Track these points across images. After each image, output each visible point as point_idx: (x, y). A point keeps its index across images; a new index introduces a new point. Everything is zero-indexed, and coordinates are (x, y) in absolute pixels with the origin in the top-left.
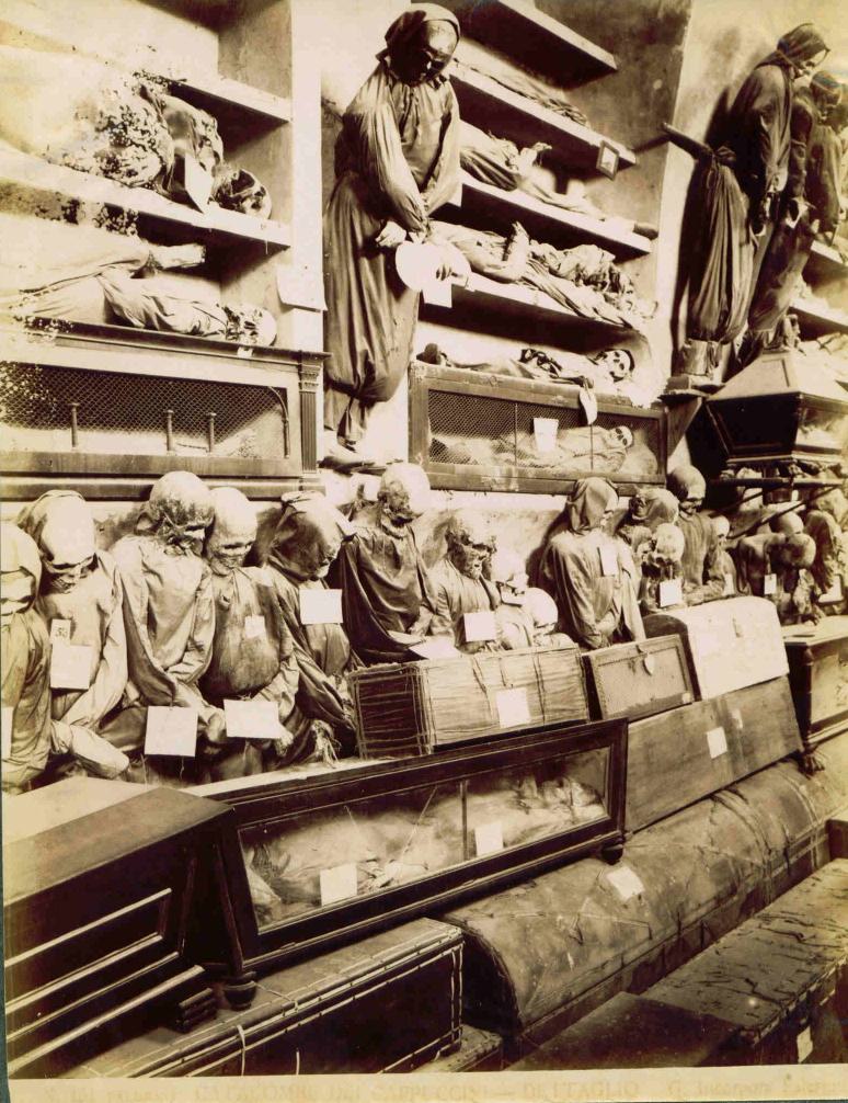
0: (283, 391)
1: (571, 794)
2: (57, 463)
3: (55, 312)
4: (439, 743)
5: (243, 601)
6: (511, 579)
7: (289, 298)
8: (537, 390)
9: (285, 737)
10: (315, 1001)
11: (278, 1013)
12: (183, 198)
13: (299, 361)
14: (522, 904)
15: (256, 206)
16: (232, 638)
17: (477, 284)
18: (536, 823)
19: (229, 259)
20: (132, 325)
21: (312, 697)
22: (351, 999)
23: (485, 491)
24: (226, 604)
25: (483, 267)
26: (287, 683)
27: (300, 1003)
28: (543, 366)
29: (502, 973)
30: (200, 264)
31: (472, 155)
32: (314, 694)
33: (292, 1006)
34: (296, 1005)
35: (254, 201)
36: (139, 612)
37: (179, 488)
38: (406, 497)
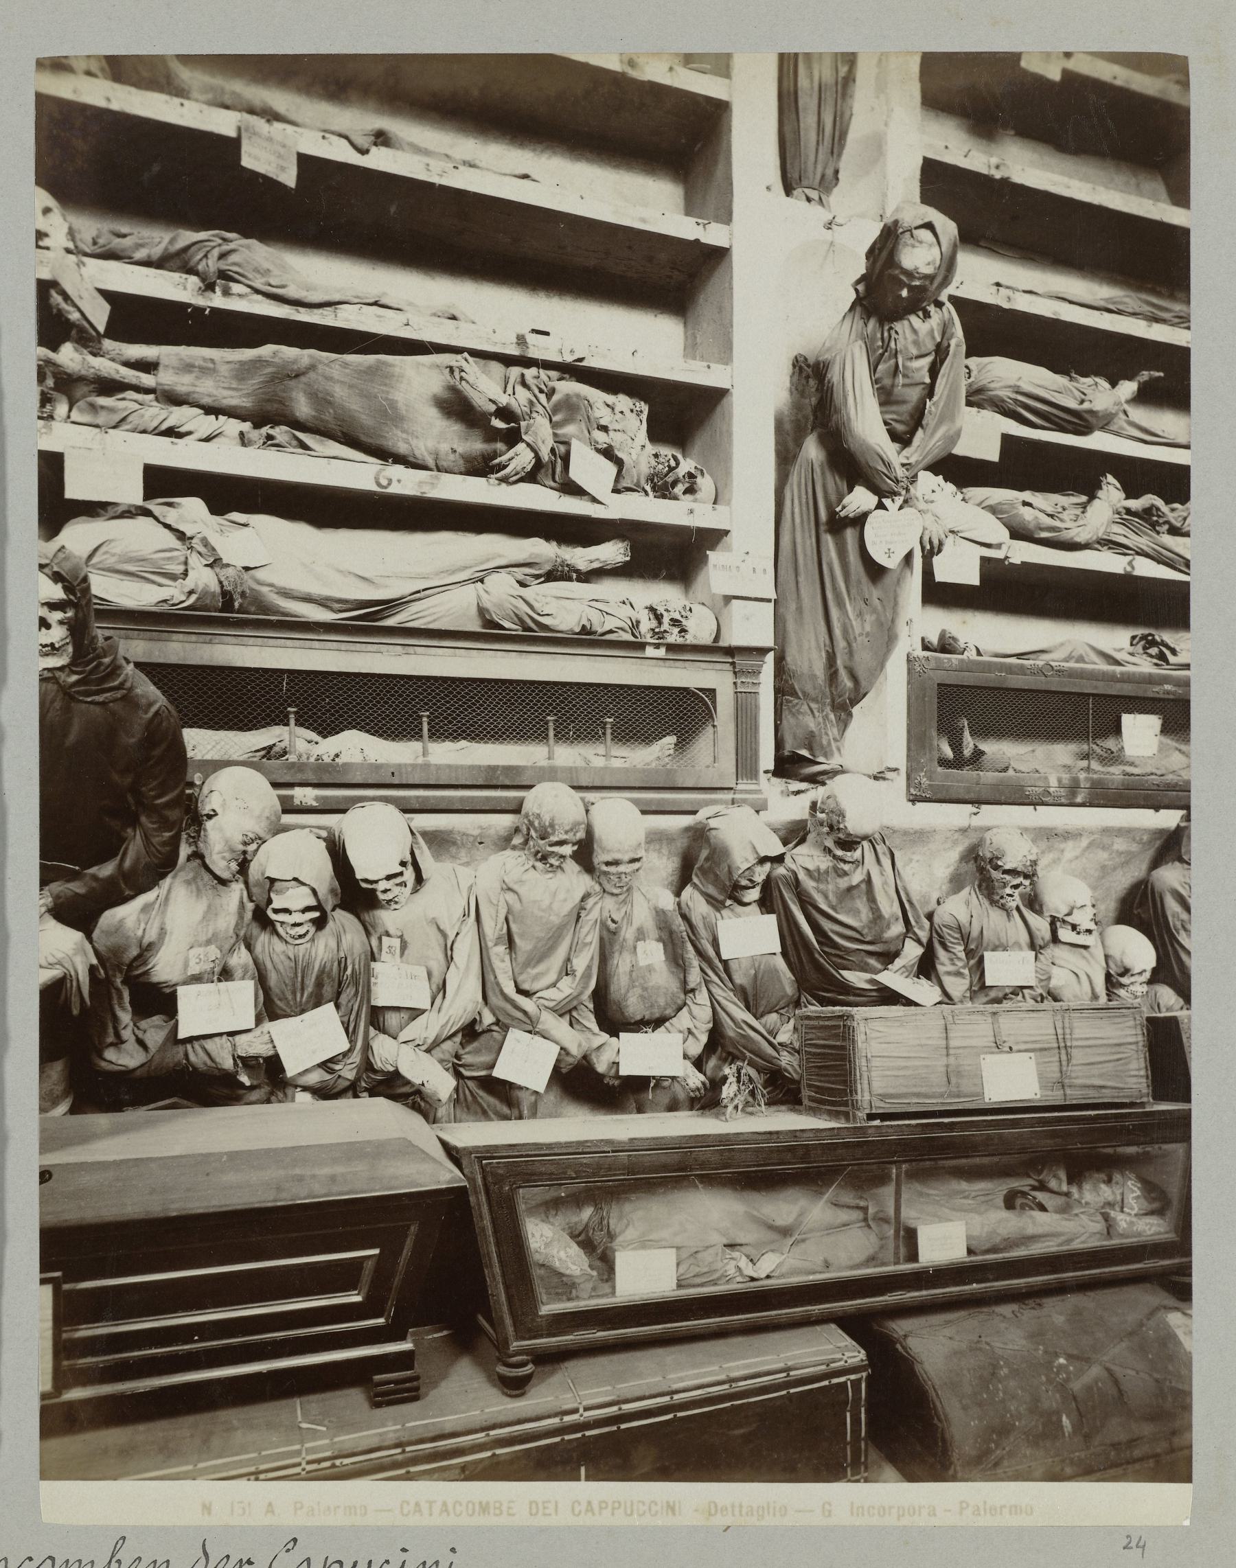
0: (712, 692)
1: (1122, 1194)
2: (401, 774)
3: (425, 620)
4: (874, 1111)
5: (636, 923)
6: (1069, 914)
7: (741, 587)
8: (1128, 679)
9: (695, 1079)
10: (665, 1400)
11: (555, 1415)
12: (572, 489)
13: (733, 657)
14: (1009, 1332)
15: (691, 490)
16: (621, 965)
17: (1023, 553)
18: (1030, 1230)
19: (671, 555)
20: (503, 628)
21: (730, 1038)
22: (557, 1439)
23: (1034, 804)
24: (612, 926)
25: (1032, 532)
26: (698, 1016)
27: (586, 1409)
28: (1150, 651)
29: (940, 1420)
30: (626, 563)
31: (1014, 396)
32: (731, 1034)
33: (575, 1411)
34: (581, 1410)
35: (687, 485)
36: (493, 928)
37: (553, 803)
38: (842, 815)
